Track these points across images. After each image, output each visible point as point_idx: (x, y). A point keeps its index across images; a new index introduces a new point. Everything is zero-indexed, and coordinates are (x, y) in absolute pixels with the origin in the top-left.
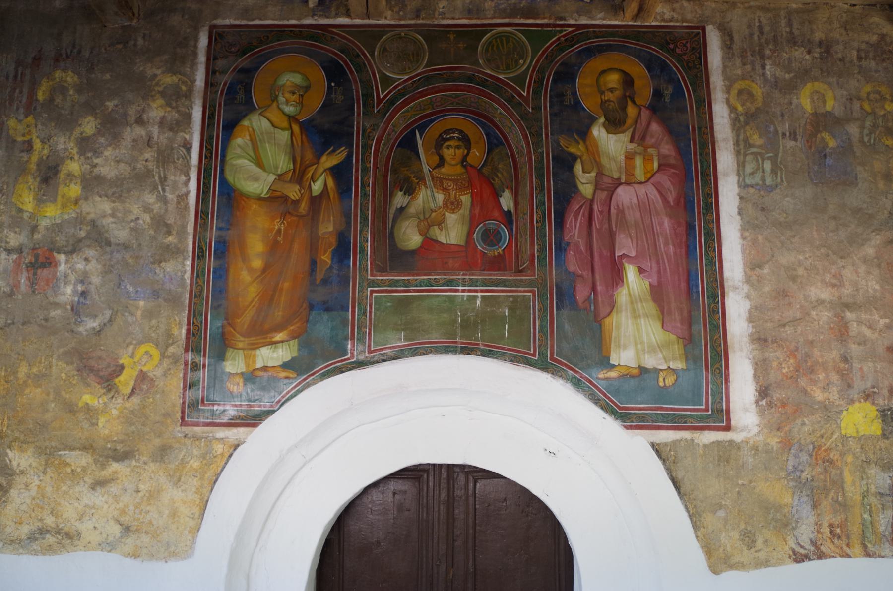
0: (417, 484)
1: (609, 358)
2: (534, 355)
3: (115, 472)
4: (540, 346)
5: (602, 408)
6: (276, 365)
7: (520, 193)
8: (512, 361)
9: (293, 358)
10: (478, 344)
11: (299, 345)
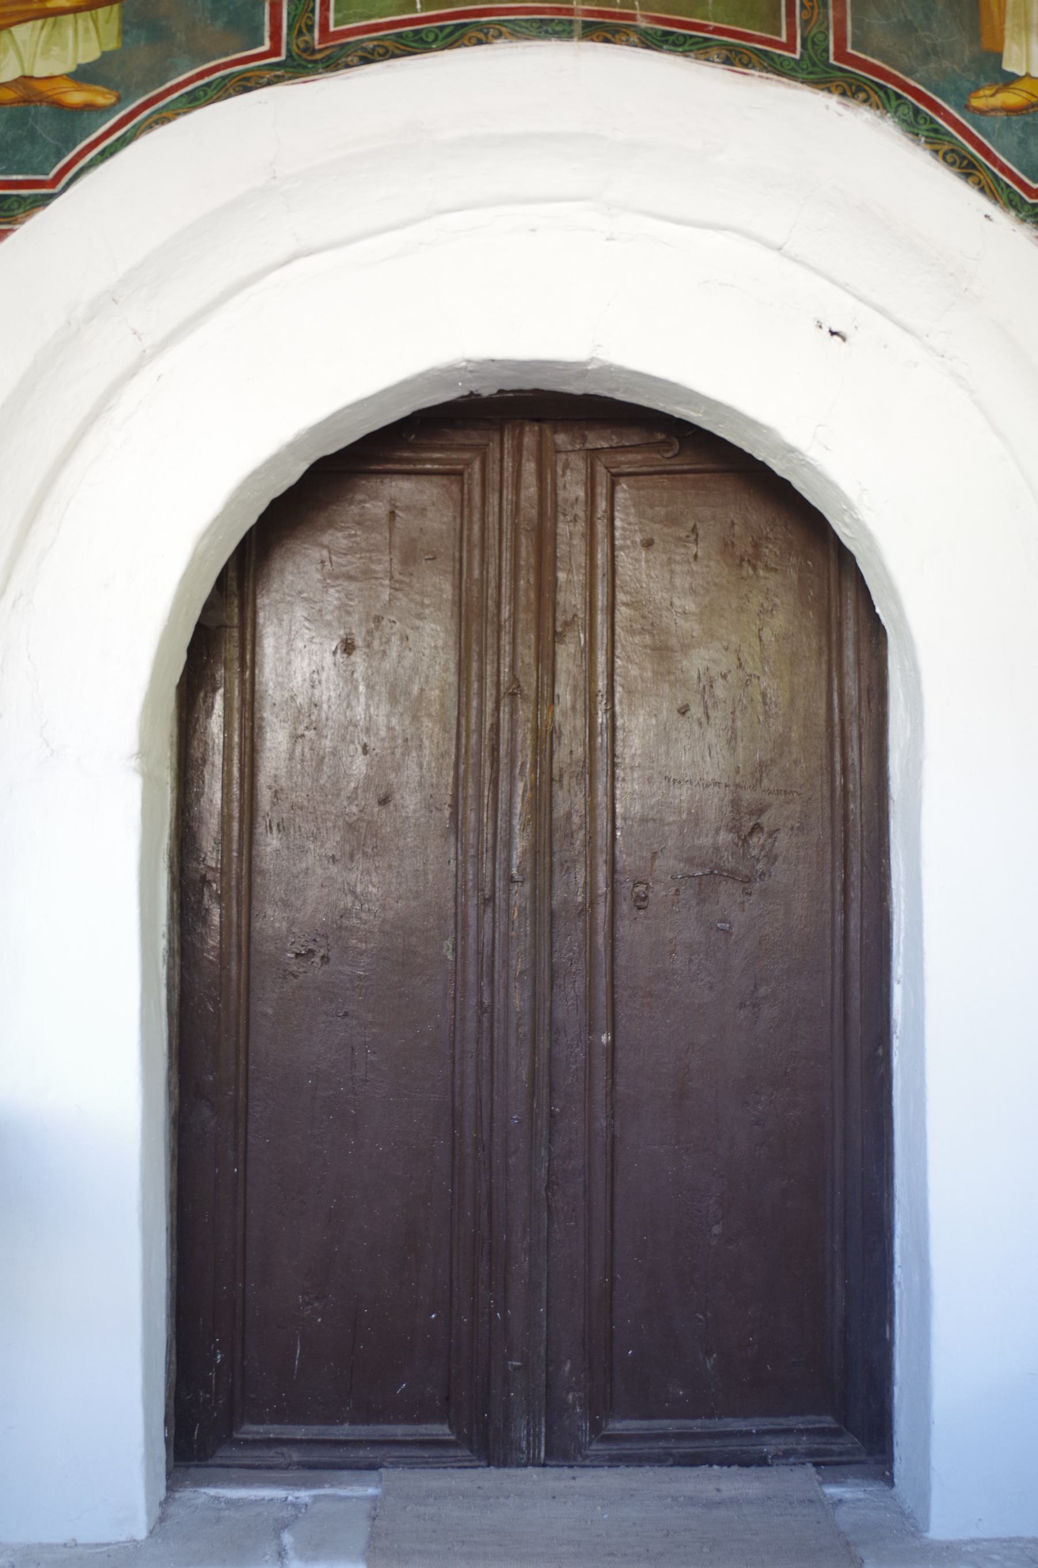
0: (455, 488)
1: (999, 56)
2: (790, 46)
3: (400, 574)
4: (805, 23)
5: (982, 190)
6: (57, 72)
7: (458, 532)
8: (727, 61)
9: (104, 55)
10: (632, 17)
11: (124, 20)
